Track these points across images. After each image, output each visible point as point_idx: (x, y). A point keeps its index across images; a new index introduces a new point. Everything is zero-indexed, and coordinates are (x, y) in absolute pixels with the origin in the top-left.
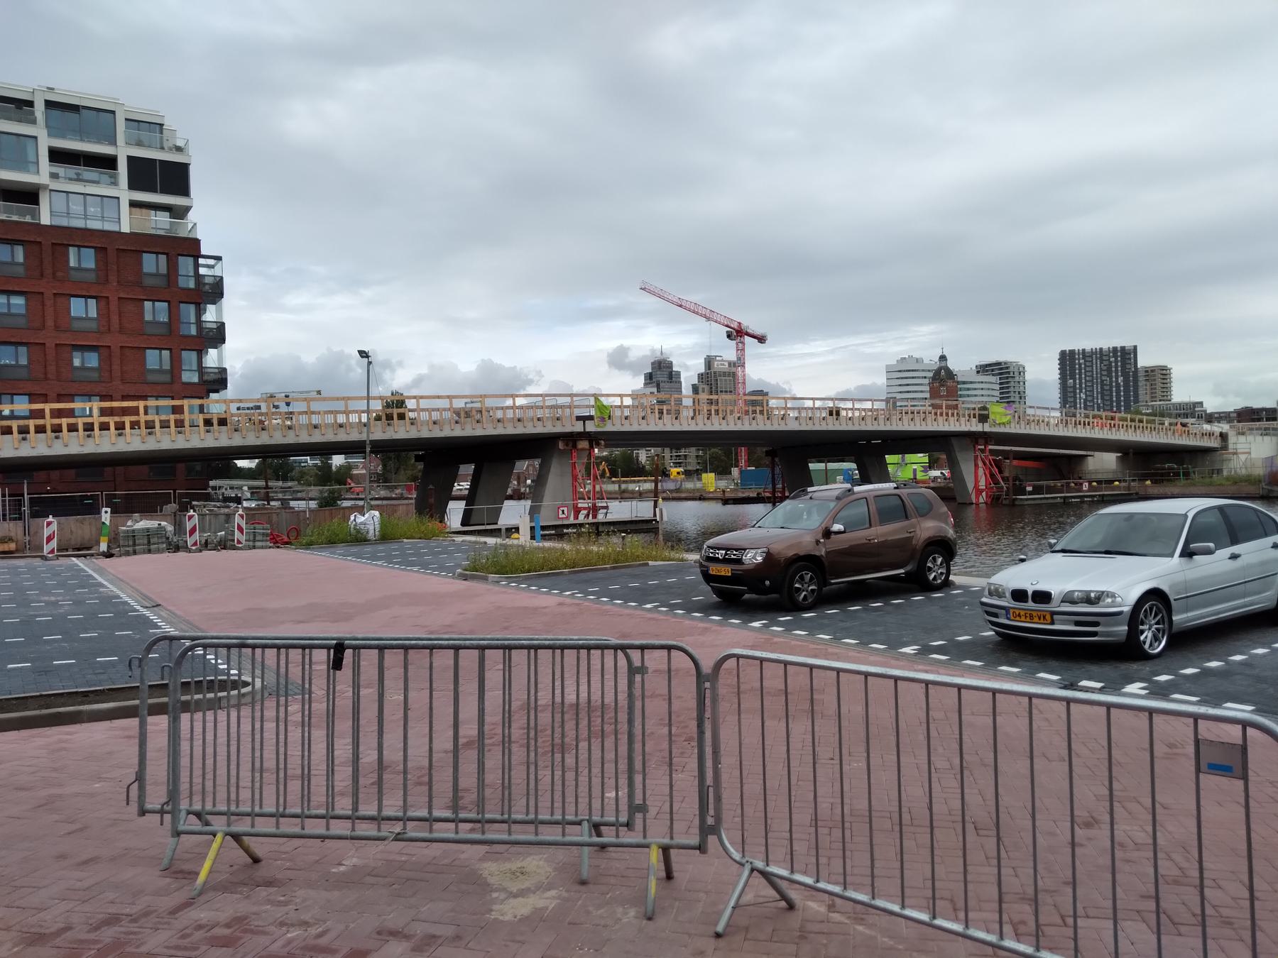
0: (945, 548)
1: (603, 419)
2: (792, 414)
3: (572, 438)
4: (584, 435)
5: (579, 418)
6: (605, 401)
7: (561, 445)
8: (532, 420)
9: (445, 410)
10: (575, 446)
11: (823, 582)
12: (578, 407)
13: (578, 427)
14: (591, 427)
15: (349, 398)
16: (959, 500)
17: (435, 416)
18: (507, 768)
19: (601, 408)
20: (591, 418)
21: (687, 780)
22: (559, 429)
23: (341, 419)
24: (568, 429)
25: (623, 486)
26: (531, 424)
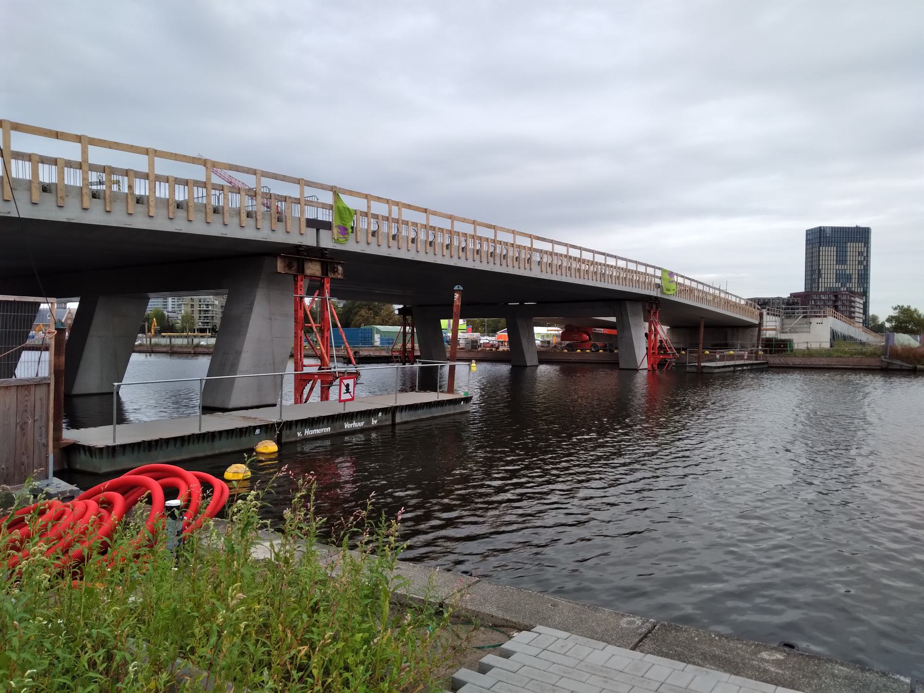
0: (35, 608)
1: (344, 230)
2: (536, 257)
3: (297, 255)
4: (318, 254)
5: (311, 223)
6: (349, 202)
7: (280, 266)
8: (238, 212)
9: (69, 164)
10: (301, 270)
11: (47, 603)
12: (309, 203)
13: (309, 239)
14: (327, 241)
15: (157, 153)
16: (622, 365)
17: (47, 175)
18: (481, 503)
19: (343, 213)
20: (327, 226)
21: (628, 461)
22: (279, 237)
23: (141, 188)
24: (294, 239)
25: (196, 341)
26: (235, 220)
